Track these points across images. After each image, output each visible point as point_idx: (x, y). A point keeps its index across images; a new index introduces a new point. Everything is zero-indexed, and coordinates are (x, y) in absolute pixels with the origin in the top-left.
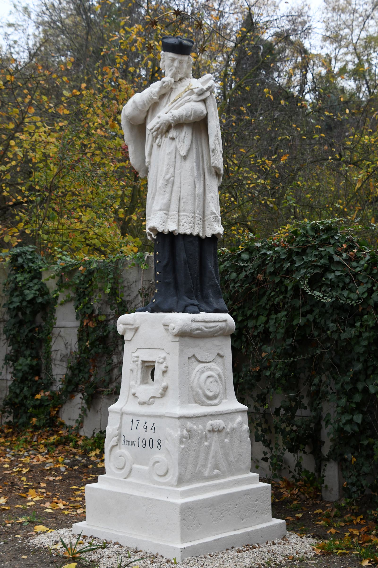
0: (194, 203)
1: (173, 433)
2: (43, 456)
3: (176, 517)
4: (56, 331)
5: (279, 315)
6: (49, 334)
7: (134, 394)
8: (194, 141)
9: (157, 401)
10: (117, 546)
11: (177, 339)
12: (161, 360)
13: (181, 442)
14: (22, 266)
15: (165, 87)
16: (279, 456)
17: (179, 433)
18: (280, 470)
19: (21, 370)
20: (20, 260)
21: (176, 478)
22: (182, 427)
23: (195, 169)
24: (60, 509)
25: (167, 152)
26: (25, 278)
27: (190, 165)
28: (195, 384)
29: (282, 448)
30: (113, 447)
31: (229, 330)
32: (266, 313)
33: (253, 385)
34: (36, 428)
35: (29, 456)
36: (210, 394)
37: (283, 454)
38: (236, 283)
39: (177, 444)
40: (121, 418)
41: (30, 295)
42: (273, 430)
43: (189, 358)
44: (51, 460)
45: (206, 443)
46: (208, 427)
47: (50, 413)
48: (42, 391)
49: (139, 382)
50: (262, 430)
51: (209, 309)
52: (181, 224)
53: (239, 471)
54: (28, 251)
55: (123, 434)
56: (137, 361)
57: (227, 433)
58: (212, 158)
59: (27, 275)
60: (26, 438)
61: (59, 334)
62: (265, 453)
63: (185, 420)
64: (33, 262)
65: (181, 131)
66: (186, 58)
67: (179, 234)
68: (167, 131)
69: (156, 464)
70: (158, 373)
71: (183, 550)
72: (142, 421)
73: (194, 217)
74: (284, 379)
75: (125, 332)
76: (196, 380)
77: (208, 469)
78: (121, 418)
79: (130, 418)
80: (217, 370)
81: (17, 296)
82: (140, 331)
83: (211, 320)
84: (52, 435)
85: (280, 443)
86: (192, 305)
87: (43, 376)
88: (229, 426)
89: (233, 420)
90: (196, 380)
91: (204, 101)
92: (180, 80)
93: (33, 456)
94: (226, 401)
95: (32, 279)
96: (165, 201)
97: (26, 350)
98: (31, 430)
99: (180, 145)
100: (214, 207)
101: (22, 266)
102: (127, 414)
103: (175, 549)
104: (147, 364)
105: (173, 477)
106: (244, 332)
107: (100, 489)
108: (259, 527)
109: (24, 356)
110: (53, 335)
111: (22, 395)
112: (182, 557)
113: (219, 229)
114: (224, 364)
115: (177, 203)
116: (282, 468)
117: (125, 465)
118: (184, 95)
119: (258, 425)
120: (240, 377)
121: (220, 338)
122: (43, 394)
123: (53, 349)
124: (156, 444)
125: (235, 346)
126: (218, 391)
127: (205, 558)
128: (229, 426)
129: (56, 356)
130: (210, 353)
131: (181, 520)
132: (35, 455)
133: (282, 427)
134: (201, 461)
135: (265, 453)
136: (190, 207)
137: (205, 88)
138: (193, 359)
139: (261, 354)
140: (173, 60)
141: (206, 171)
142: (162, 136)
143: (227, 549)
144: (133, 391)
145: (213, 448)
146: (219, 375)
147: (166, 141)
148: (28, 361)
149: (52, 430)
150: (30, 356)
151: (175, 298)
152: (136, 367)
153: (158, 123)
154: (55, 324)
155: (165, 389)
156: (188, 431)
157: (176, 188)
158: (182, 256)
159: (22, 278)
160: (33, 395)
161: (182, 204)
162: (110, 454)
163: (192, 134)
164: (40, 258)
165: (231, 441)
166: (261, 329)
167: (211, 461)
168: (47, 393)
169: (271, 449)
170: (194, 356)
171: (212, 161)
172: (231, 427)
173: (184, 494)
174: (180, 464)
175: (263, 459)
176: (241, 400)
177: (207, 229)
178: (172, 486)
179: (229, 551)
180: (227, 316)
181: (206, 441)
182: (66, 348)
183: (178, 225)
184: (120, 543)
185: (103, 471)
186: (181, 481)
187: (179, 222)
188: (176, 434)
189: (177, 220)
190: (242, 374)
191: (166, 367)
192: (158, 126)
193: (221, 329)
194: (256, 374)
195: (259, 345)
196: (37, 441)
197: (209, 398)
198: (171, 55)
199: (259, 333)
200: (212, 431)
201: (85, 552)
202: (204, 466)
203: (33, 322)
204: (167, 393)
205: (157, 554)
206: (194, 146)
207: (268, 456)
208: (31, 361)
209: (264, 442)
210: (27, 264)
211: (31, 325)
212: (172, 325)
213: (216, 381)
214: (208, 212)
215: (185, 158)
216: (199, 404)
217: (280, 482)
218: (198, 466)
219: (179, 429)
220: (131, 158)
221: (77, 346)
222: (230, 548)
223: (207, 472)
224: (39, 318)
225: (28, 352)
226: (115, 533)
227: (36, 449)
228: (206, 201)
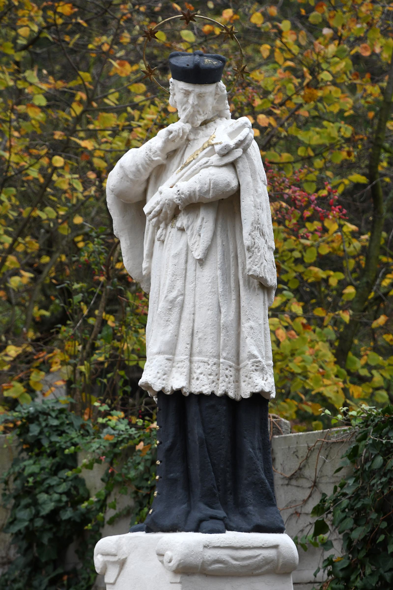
0: (218, 340)
8: (219, 233)
11: (178, 579)
14: (37, 443)
15: (173, 140)
20: (34, 429)
23: (220, 281)
25: (173, 252)
26: (42, 469)
27: (211, 273)
41: (47, 503)
52: (195, 376)
58: (248, 261)
59: (46, 462)
64: (61, 433)
65: (197, 216)
66: (210, 89)
67: (191, 394)
68: (175, 216)
73: (217, 364)
81: (27, 506)
83: (245, 544)
86: (213, 518)
91: (233, 165)
92: (205, 123)
95: (56, 470)
96: (167, 337)
99: (193, 241)
100: (257, 343)
101: (37, 443)
113: (266, 383)
115: (188, 340)
118: (201, 155)
121: (267, 579)
136: (209, 347)
137: (232, 143)
140: (187, 94)
141: (241, 283)
142: (166, 225)
147: (172, 232)
153: (158, 203)
157: (186, 315)
158: (196, 431)
159: (35, 469)
161: (196, 342)
163: (216, 221)
164: (77, 423)
171: (248, 267)
177: (243, 384)
183: (190, 379)
187: (191, 372)
189: (186, 370)
192: (158, 208)
193: (267, 561)
198: (182, 85)
203: (59, 560)
206: (219, 241)
211: (55, 569)
212: (168, 554)
214: (244, 355)
215: (201, 262)
220: (125, 259)
228: (242, 336)
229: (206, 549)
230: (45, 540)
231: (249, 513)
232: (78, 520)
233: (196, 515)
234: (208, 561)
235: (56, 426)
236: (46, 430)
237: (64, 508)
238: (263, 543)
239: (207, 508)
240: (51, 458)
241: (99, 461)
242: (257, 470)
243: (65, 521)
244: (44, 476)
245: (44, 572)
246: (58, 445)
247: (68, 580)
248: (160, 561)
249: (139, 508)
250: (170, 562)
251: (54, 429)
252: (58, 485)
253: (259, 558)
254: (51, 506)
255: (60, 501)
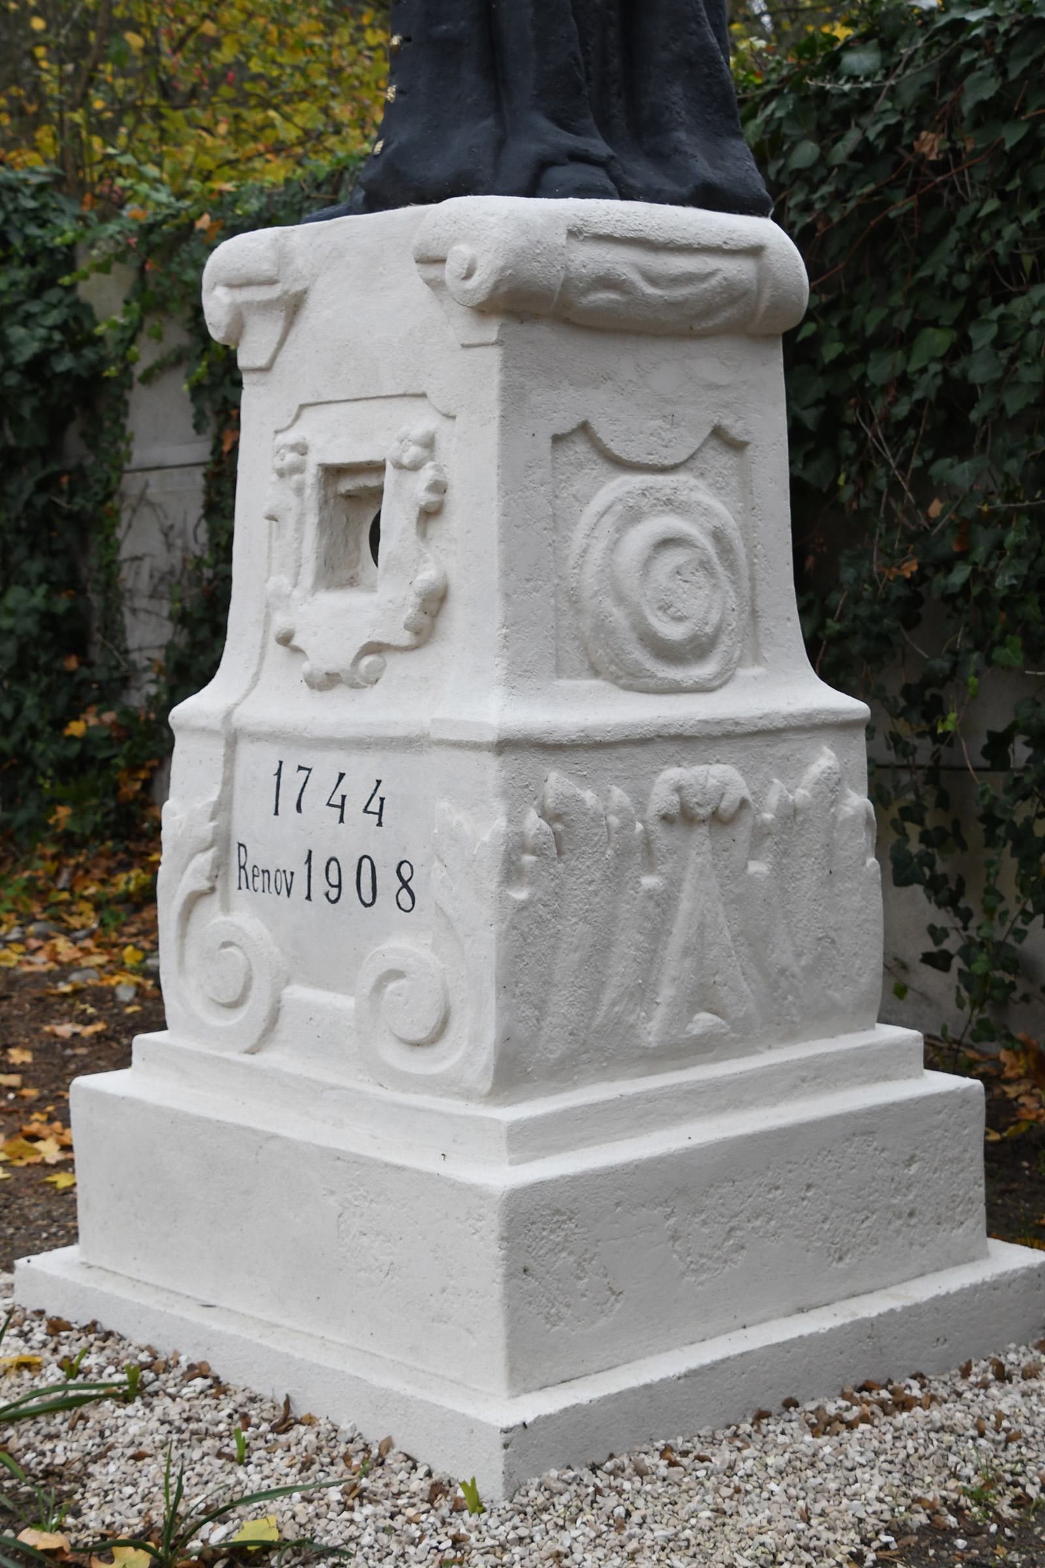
1: (463, 825)
2: (75, 941)
3: (483, 1257)
4: (131, 485)
5: (1018, 305)
6: (109, 496)
7: (285, 640)
9: (396, 665)
10: (199, 1383)
11: (491, 331)
12: (412, 452)
13: (512, 872)
16: (1001, 945)
17: (501, 823)
18: (1002, 1005)
19: (11, 632)
21: (486, 1056)
22: (518, 795)
24: (44, 1165)
26: (14, 284)
28: (589, 579)
29: (1014, 911)
30: (194, 899)
31: (776, 306)
32: (951, 311)
33: (884, 639)
34: (69, 842)
35: (21, 941)
36: (674, 632)
37: (1020, 935)
38: (814, 189)
39: (491, 884)
40: (230, 760)
42: (975, 832)
43: (557, 439)
44: (101, 959)
45: (649, 881)
46: (661, 797)
47: (116, 789)
48: (94, 709)
49: (308, 578)
50: (924, 838)
51: (670, 187)
53: (826, 1017)
54: (25, 182)
55: (238, 836)
56: (298, 469)
57: (761, 833)
59: (21, 274)
60: (32, 880)
61: (142, 498)
62: (937, 934)
63: (532, 760)
64: (43, 224)
69: (392, 986)
70: (397, 516)
71: (517, 1438)
72: (325, 766)
74: (1034, 598)
75: (238, 325)
76: (596, 554)
77: (660, 1013)
78: (230, 760)
79: (269, 756)
80: (707, 512)
82: (313, 317)
83: (679, 237)
84: (126, 867)
85: (1008, 885)
86: (578, 157)
87: (95, 653)
88: (773, 799)
89: (791, 769)
90: (596, 554)
93: (34, 943)
94: (757, 671)
97: (31, 555)
98: (51, 850)
102: (255, 737)
103: (472, 1427)
104: (347, 485)
105: (472, 1048)
106: (851, 415)
107: (133, 1103)
108: (923, 1290)
109: (27, 584)
110: (122, 500)
111: (22, 724)
112: (508, 1474)
114: (746, 488)
116: (1016, 995)
117: (247, 987)
119: (907, 814)
120: (828, 612)
122: (93, 721)
123: (125, 553)
124: (388, 882)
125: (808, 476)
126: (714, 617)
127: (641, 1472)
128: (773, 799)
129: (136, 580)
130: (673, 421)
131: (509, 1276)
132: (47, 937)
133: (1019, 820)
134: (621, 969)
135: (937, 934)
138: (581, 448)
139: (924, 504)
143: (761, 1415)
144: (280, 622)
145: (685, 905)
146: (718, 536)
148: (38, 599)
149: (127, 850)
150: (42, 579)
151: (489, 122)
152: (293, 501)
154: (129, 456)
155: (435, 602)
156: (551, 816)
160: (59, 724)
162: (183, 935)
165: (778, 869)
166: (926, 387)
167: (674, 969)
168: (109, 717)
169: (966, 916)
170: (584, 428)
172: (783, 803)
173: (525, 1140)
174: (504, 987)
175: (928, 959)
176: (831, 661)
178: (467, 1095)
179: (771, 1426)
180: (763, 229)
181: (650, 865)
182: (169, 546)
184: (216, 1369)
185: (153, 1018)
186: (513, 1072)
188: (486, 827)
190: (838, 600)
191: (438, 487)
193: (733, 294)
194: (900, 591)
195: (916, 462)
196: (71, 890)
197: (668, 652)
199: (920, 404)
200: (683, 817)
201: (33, 1415)
202: (642, 992)
203: (51, 450)
204: (443, 623)
205: (388, 1445)
207: (952, 944)
208: (47, 597)
209: (934, 886)
210: (20, 230)
211: (44, 464)
213: (705, 565)
216: (615, 679)
217: (1004, 1056)
218: (609, 995)
219: (499, 806)
221: (203, 537)
222: (775, 1407)
223: (654, 1026)
224: (74, 444)
225: (35, 567)
226: (195, 1316)
227: (58, 919)
229: (575, 244)
230: (26, 410)
231: (676, 150)
232: (85, 374)
233: (526, 149)
234: (581, 278)
235: (33, 210)
236: (15, 217)
237: (58, 352)
238: (725, 237)
239: (556, 128)
240: (28, 267)
241: (120, 257)
242: (696, 19)
243: (61, 374)
244: (17, 298)
245: (25, 471)
246: (39, 241)
247: (70, 482)
248: (428, 282)
249: (201, 346)
250: (468, 276)
251: (31, 215)
252: (44, 313)
253: (714, 281)
254: (34, 347)
255: (49, 339)
